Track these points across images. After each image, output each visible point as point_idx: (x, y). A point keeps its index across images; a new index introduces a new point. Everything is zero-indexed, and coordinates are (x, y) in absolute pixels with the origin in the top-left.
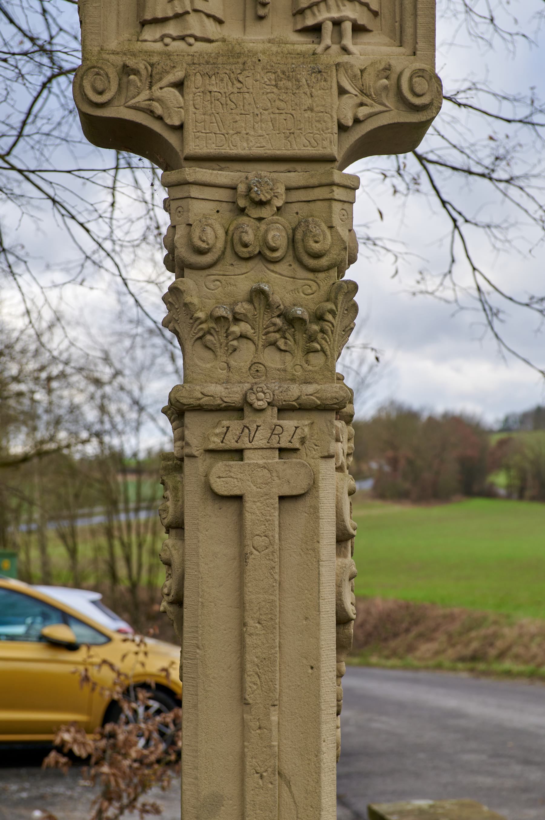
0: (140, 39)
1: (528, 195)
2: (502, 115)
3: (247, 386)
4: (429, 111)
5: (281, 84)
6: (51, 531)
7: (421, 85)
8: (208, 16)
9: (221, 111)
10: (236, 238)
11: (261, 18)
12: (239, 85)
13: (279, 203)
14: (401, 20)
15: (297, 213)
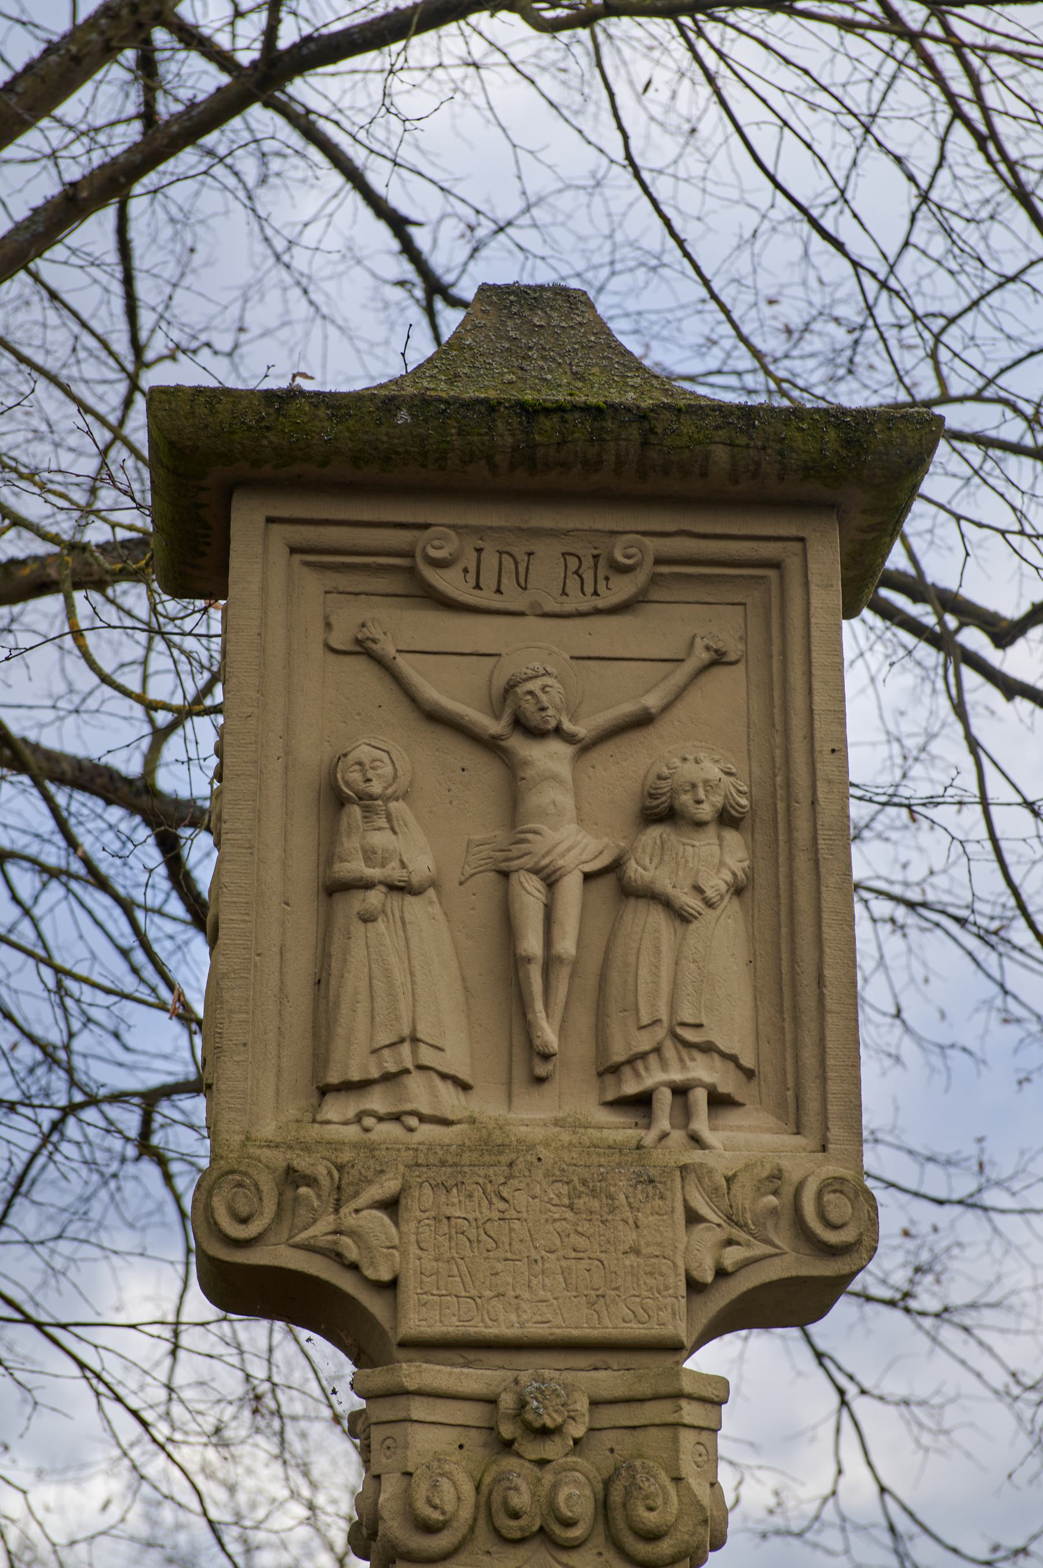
0: (319, 1118)
1: (981, 1343)
2: (925, 1190)
4: (855, 1255)
5: (579, 1203)
7: (839, 1207)
8: (444, 1076)
9: (468, 1253)
10: (497, 1499)
11: (540, 1080)
12: (502, 1206)
13: (577, 1430)
14: (798, 1086)
15: (612, 1450)
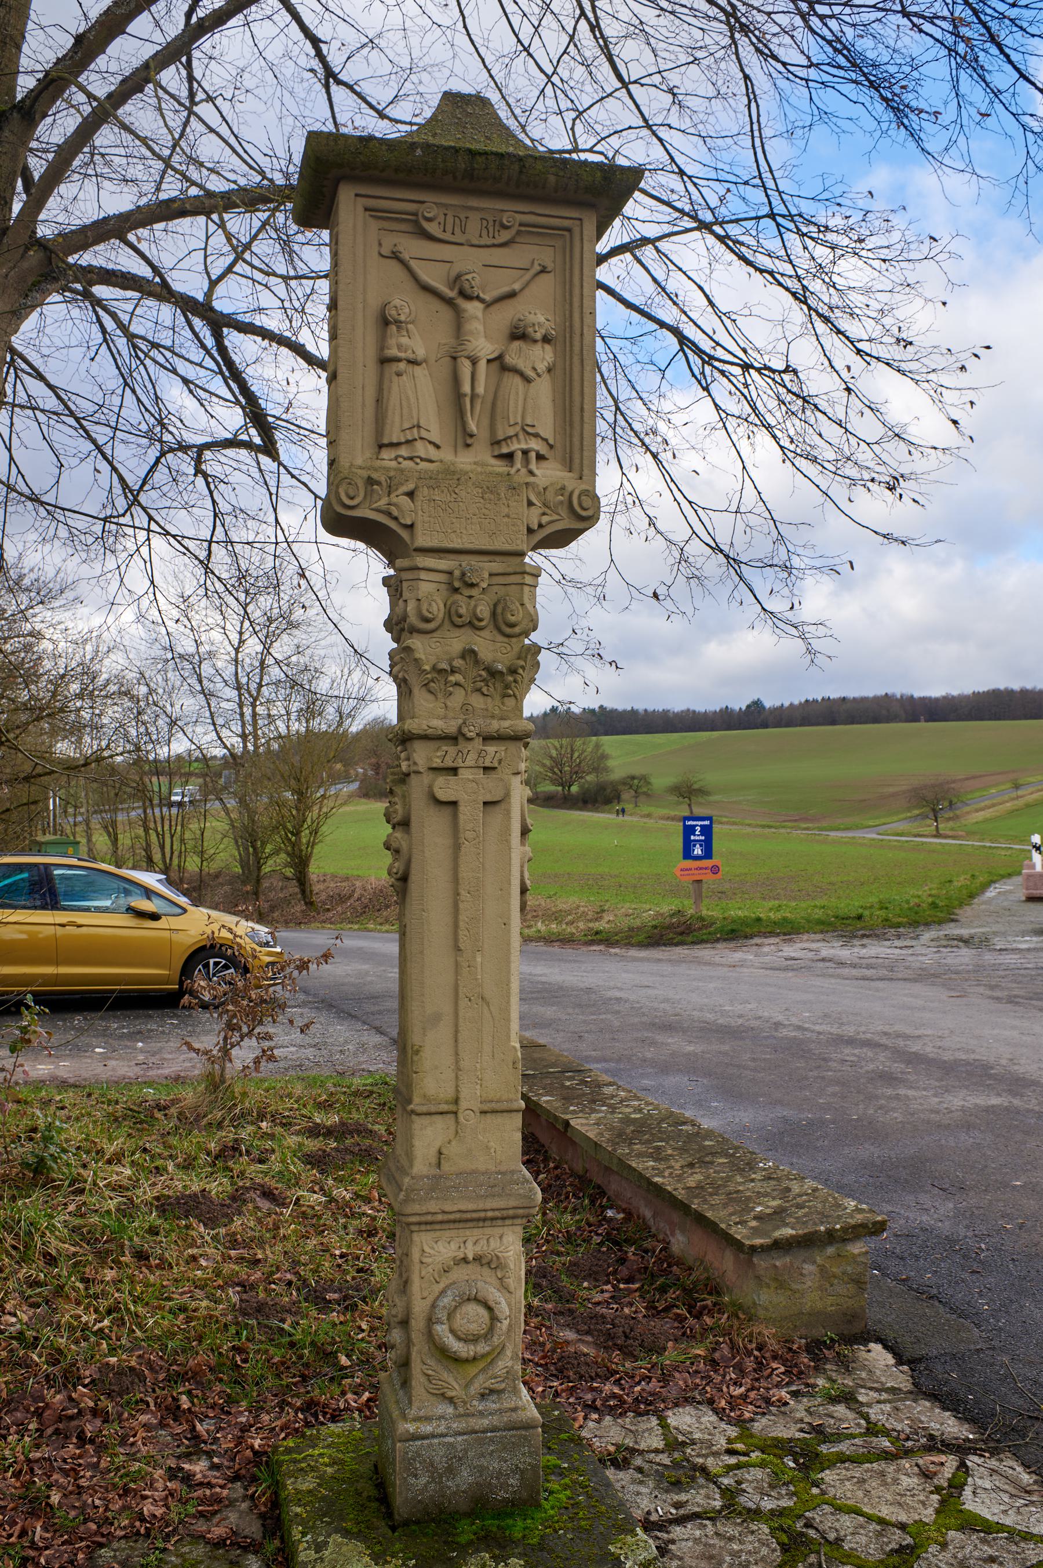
3: (460, 721)
6: (95, 822)
7: (587, 502)
8: (430, 442)
11: (468, 446)
13: (484, 585)
14: (571, 452)
